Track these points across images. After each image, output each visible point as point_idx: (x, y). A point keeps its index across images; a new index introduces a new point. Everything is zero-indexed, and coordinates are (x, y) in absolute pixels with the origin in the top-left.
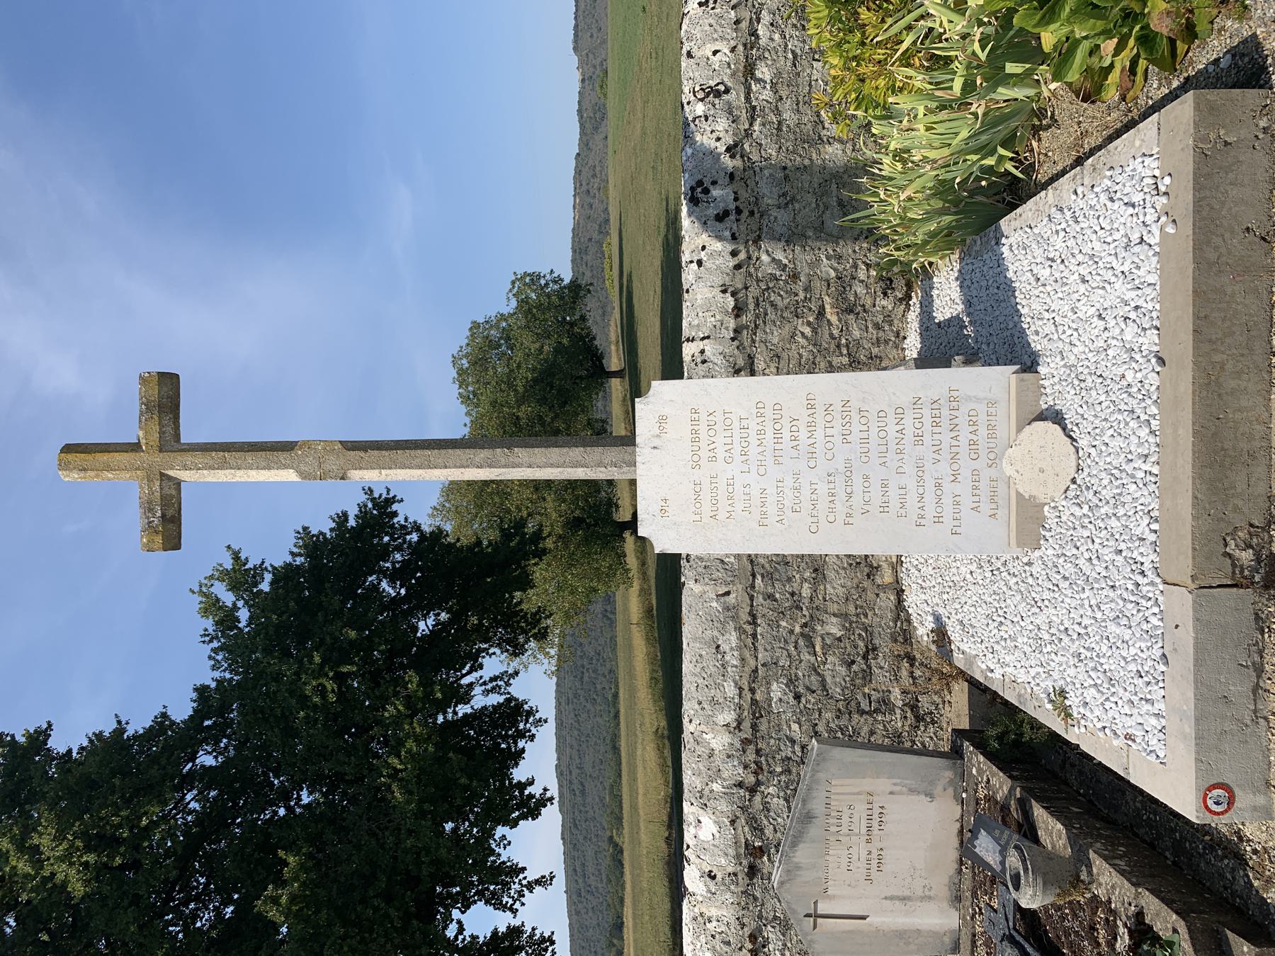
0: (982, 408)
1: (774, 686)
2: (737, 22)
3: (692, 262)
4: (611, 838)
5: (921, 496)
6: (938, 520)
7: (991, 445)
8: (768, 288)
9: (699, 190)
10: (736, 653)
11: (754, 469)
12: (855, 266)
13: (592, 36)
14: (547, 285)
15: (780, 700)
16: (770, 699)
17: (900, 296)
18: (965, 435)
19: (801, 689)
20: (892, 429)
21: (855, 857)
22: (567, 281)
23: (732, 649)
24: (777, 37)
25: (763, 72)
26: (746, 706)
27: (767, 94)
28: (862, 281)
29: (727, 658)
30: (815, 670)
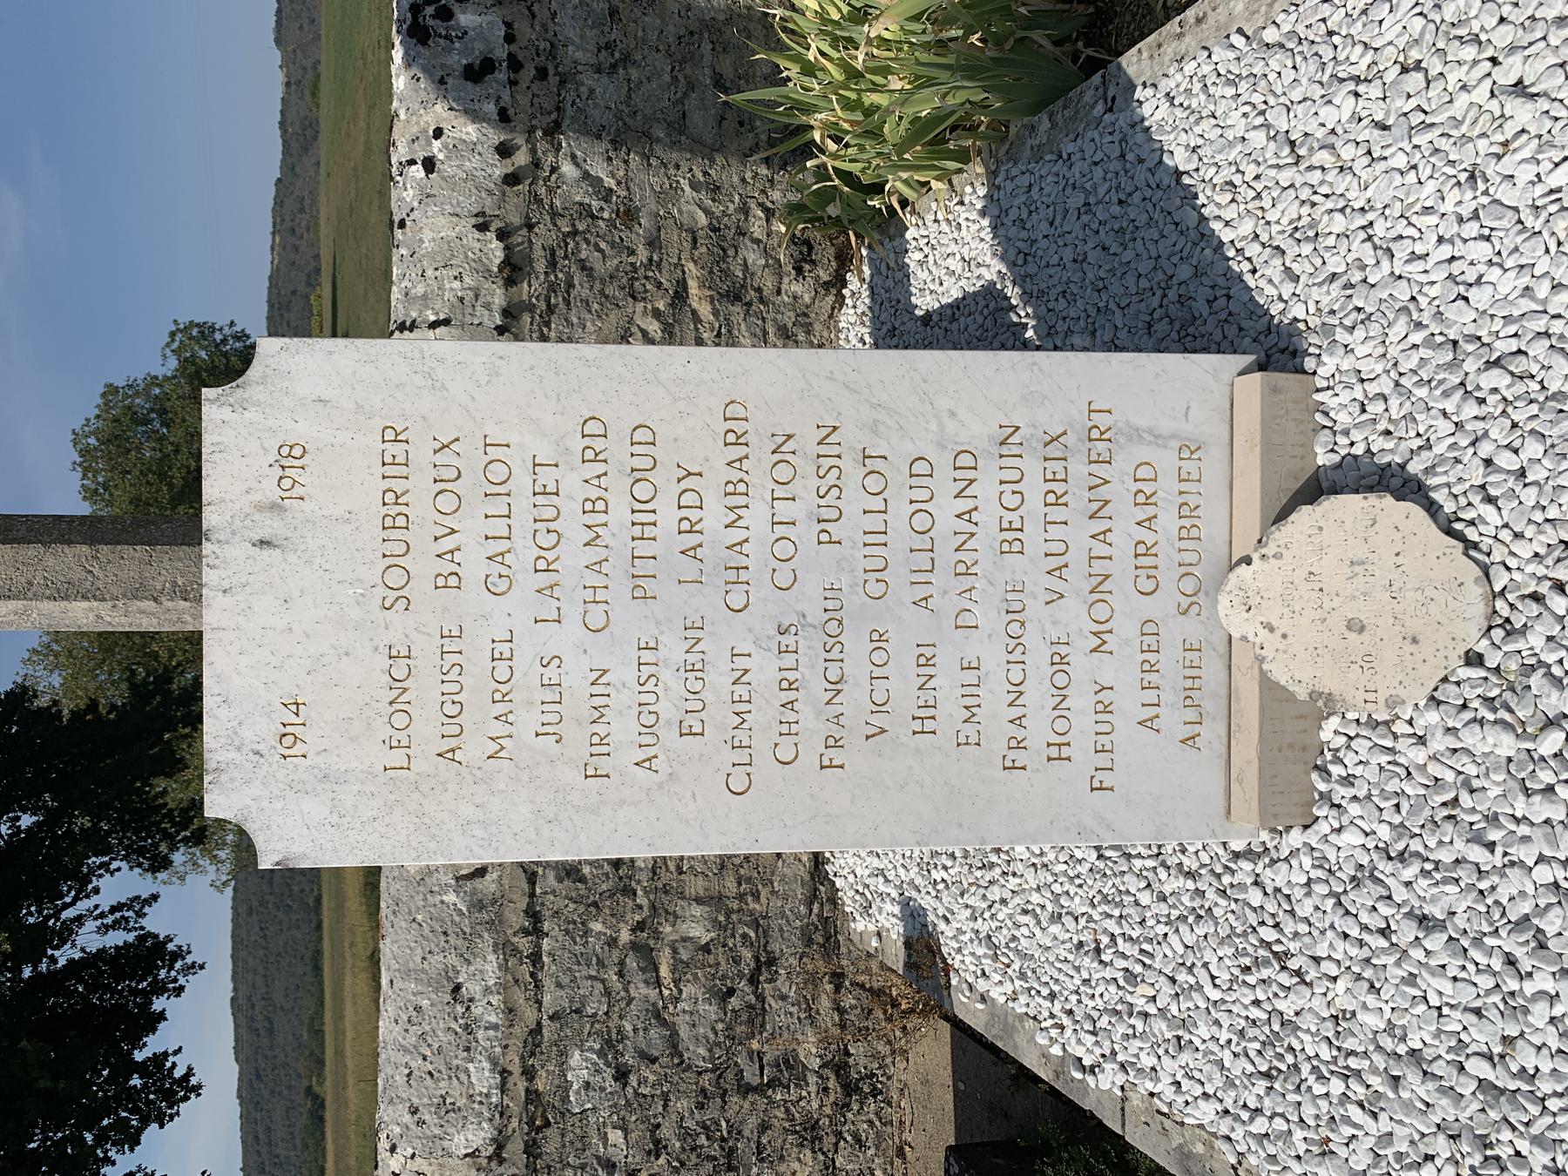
0: (1166, 460)
1: (576, 1058)
3: (412, 162)
4: (309, 1090)
5: (1018, 690)
6: (1058, 753)
7: (1190, 557)
8: (575, 233)
9: (430, 10)
10: (495, 1000)
11: (573, 612)
12: (745, 210)
13: (301, 28)
14: (224, 341)
15: (587, 1085)
16: (566, 1086)
17: (825, 277)
19: (629, 1059)
20: (946, 509)
26: (515, 1108)
28: (757, 241)
29: (477, 1010)
30: (658, 1016)
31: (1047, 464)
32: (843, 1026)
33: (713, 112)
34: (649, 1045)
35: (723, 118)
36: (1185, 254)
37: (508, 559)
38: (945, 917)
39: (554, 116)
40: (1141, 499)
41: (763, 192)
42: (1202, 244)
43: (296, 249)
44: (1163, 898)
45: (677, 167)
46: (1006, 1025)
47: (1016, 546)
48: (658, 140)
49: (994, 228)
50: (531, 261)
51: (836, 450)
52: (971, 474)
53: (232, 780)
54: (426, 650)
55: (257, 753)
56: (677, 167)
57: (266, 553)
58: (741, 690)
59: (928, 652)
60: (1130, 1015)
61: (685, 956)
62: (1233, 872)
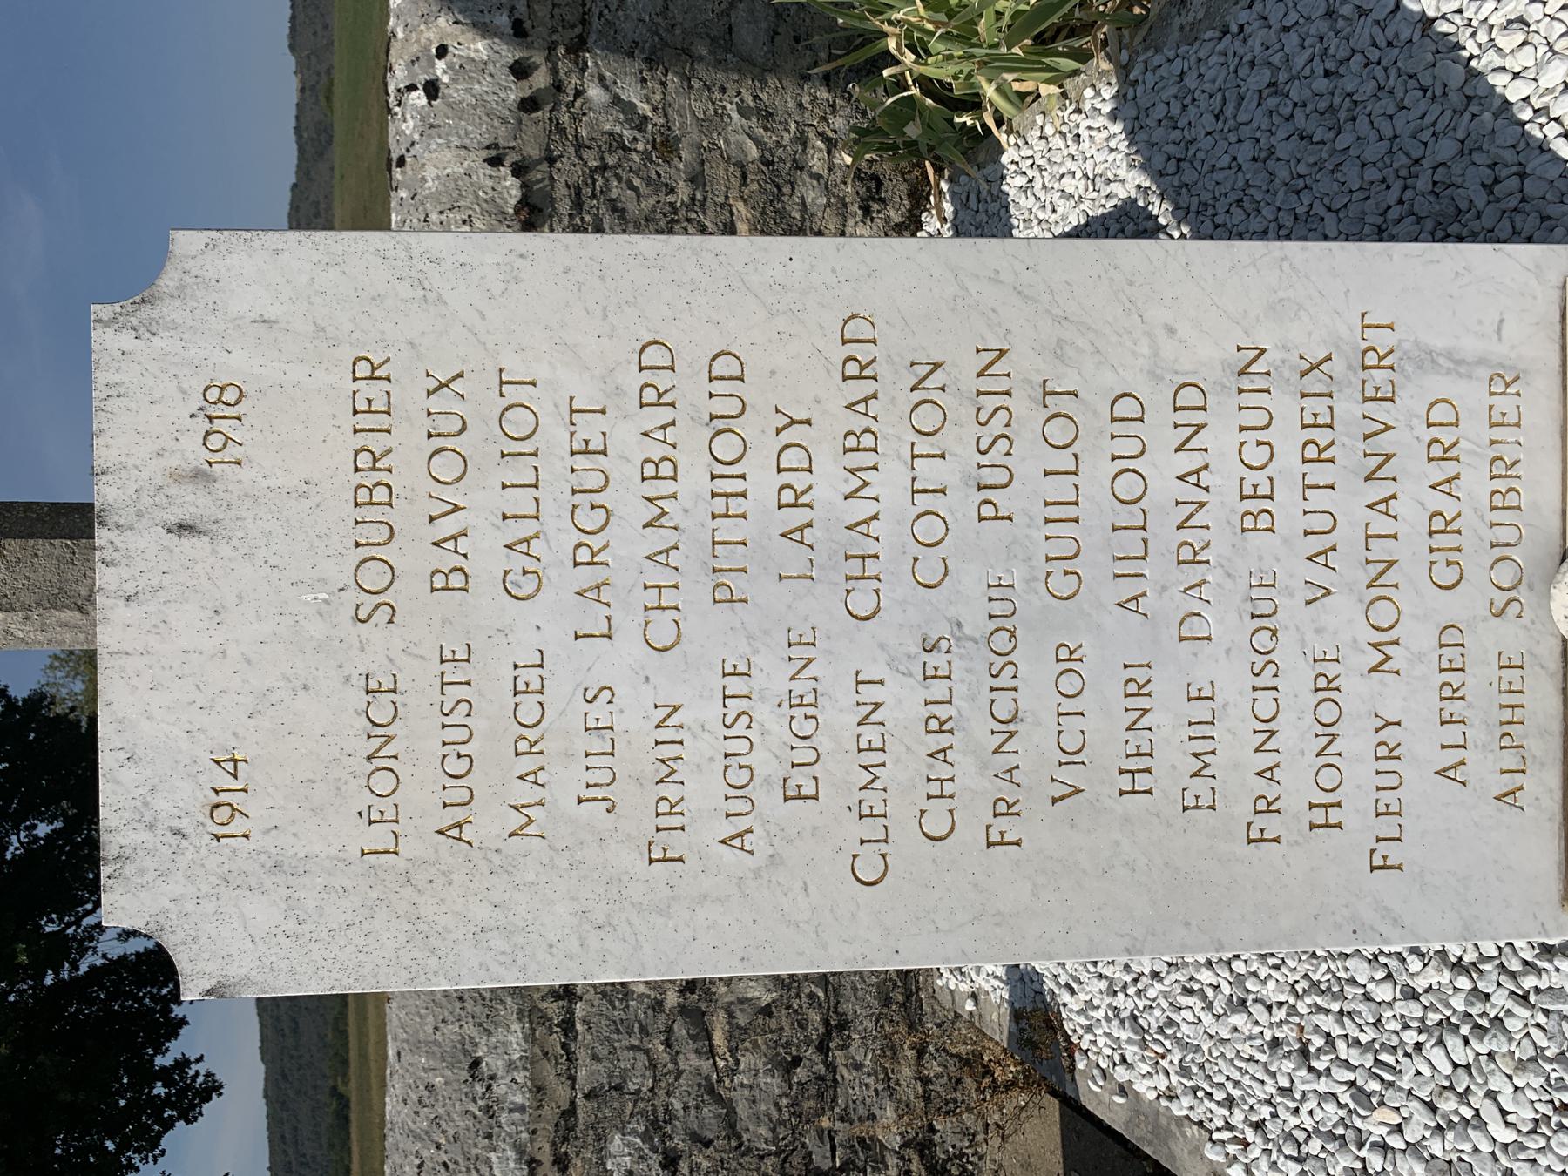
0: (1471, 395)
3: (412, 88)
4: (334, 1088)
8: (604, 167)
11: (628, 624)
12: (802, 140)
13: (315, 34)
17: (896, 218)
18: (1415, 501)
19: (679, 1142)
20: (1163, 469)
23: (511, 1066)
28: (818, 177)
29: (500, 1089)
30: (711, 1090)
31: (1306, 402)
32: (927, 1098)
33: (764, 25)
34: (702, 1127)
35: (776, 33)
36: (1440, 127)
37: (536, 547)
38: (1068, 986)
39: (578, 30)
40: (1437, 451)
41: (824, 119)
42: (1474, 108)
44: (1413, 995)
45: (723, 90)
46: (1157, 1126)
47: (1264, 521)
48: (701, 59)
49: (1131, 134)
50: (553, 201)
51: (1004, 384)
52: (1198, 418)
53: (142, 872)
54: (419, 678)
55: (177, 832)
56: (723, 90)
57: (187, 542)
58: (870, 734)
59: (1140, 675)
60: (1361, 1145)
61: (742, 1020)
62: (1539, 972)
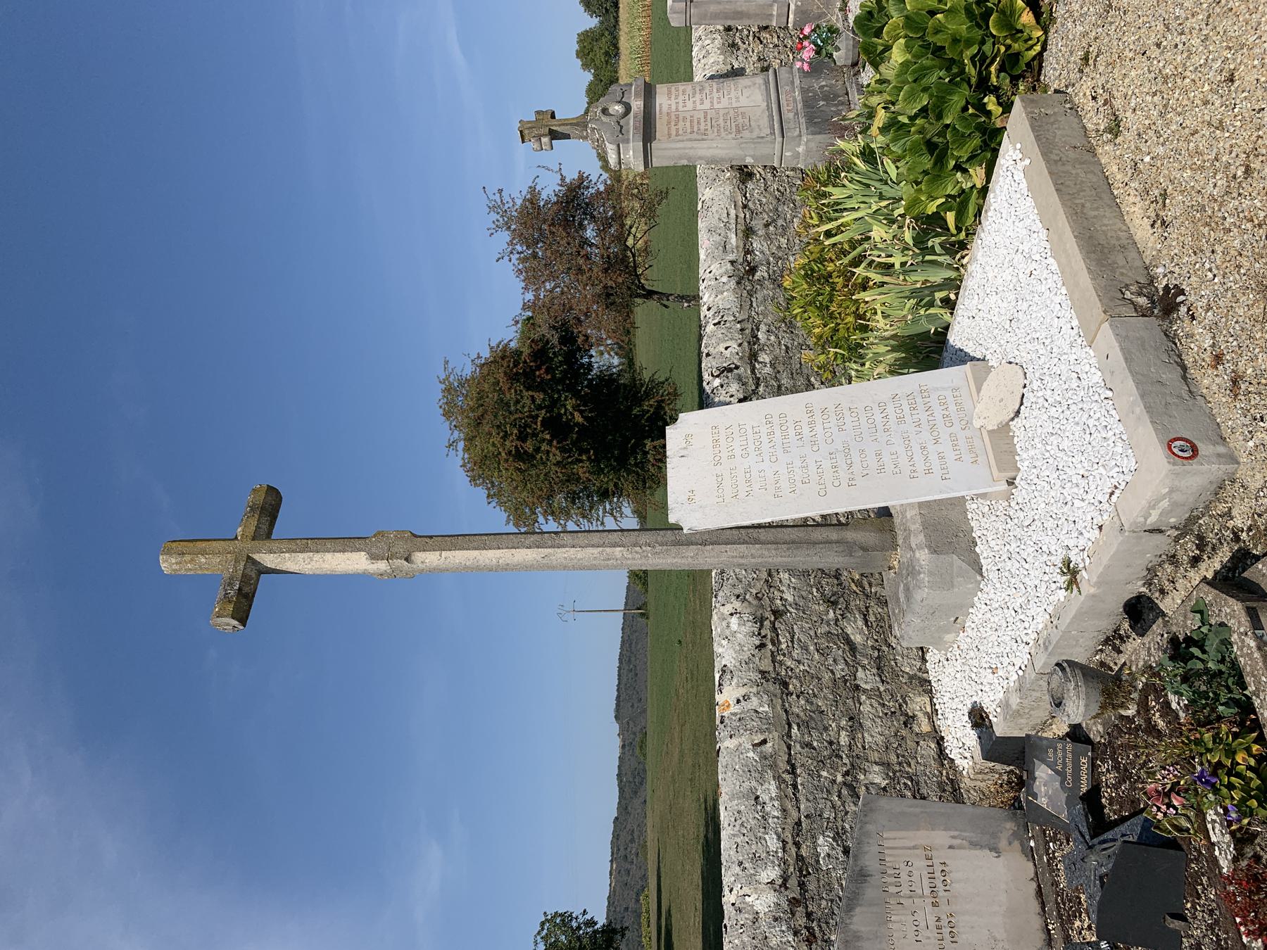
0: (949, 393)
1: (821, 840)
2: (742, 330)
10: (776, 803)
11: (766, 458)
13: (632, 706)
14: (579, 928)
15: (829, 855)
16: (818, 855)
18: (938, 413)
21: (923, 924)
22: (601, 920)
23: (771, 799)
24: (772, 338)
25: (764, 357)
26: (791, 861)
27: (768, 370)
29: (768, 809)
43: (628, 872)
